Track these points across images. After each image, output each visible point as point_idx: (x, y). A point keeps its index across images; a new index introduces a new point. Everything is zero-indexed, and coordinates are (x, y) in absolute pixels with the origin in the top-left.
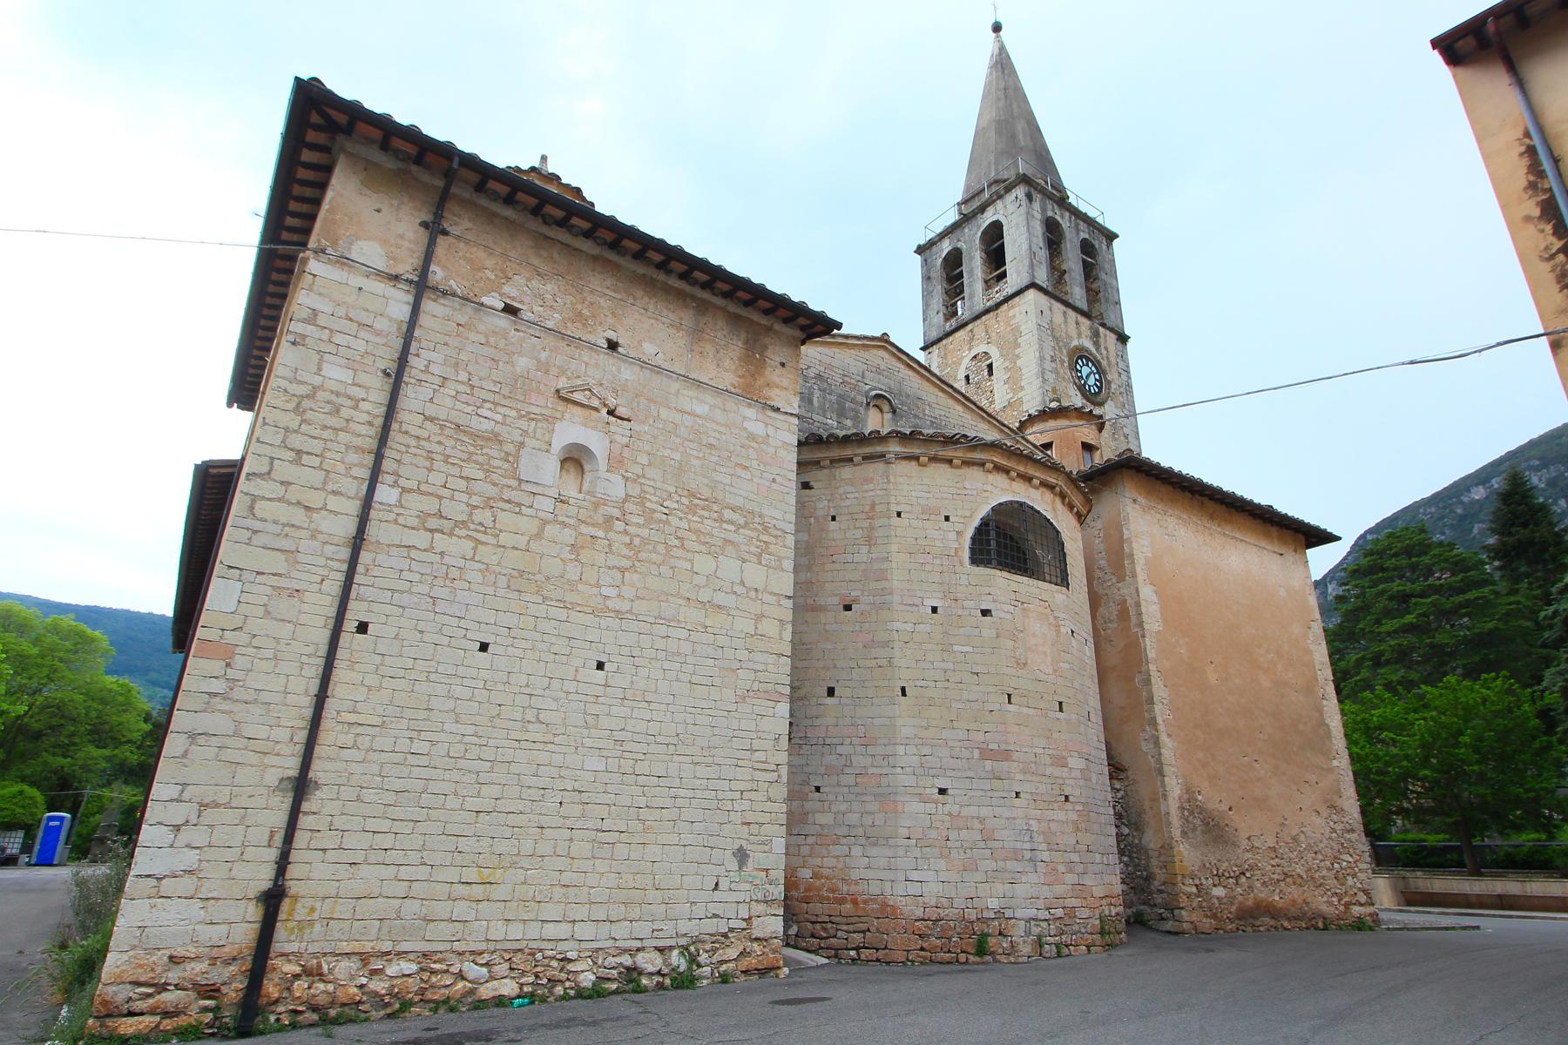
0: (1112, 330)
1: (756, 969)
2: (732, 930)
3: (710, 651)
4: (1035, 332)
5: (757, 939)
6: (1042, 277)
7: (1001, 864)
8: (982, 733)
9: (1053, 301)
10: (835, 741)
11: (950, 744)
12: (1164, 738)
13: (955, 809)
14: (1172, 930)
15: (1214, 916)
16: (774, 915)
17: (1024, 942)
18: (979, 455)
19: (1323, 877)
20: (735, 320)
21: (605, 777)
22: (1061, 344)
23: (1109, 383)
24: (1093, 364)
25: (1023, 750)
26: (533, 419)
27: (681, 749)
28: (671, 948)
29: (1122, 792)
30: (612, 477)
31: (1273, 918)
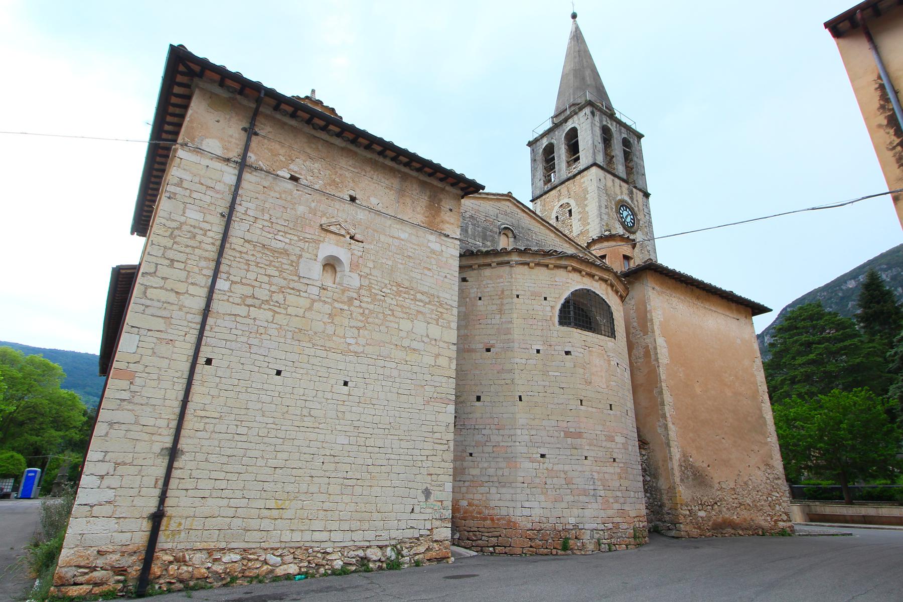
0: (640, 190)
1: (435, 558)
2: (421, 536)
3: (409, 375)
4: (596, 191)
5: (436, 541)
6: (600, 159)
7: (576, 498)
8: (565, 422)
9: (606, 174)
10: (481, 427)
11: (547, 428)
12: (670, 425)
13: (550, 466)
14: (675, 536)
15: (699, 528)
16: (446, 527)
17: (590, 543)
18: (564, 262)
19: (762, 505)
20: (423, 184)
21: (349, 448)
22: (611, 198)
23: (639, 220)
24: (630, 210)
25: (589, 432)
26: (307, 242)
27: (392, 432)
28: (386, 546)
29: (646, 457)
30: (352, 275)
31: (733, 529)
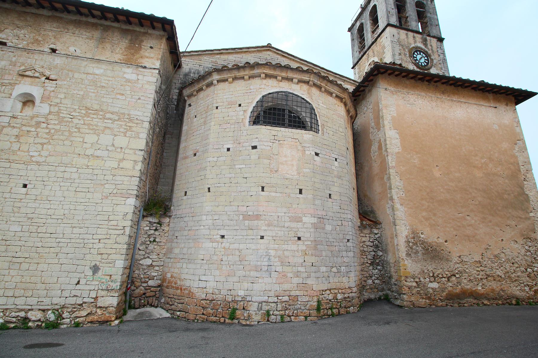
0: (434, 37)
1: (97, 321)
2: (85, 303)
3: (89, 177)
4: (390, 45)
6: (394, 20)
9: (400, 30)
12: (398, 206)
15: (429, 298)
16: (112, 296)
18: (256, 71)
19: (518, 276)
20: (125, 32)
21: (21, 234)
22: (404, 47)
23: (432, 60)
24: (423, 53)
26: (4, 85)
27: (65, 221)
28: (48, 310)
29: (379, 235)
30: (42, 105)
31: (475, 299)
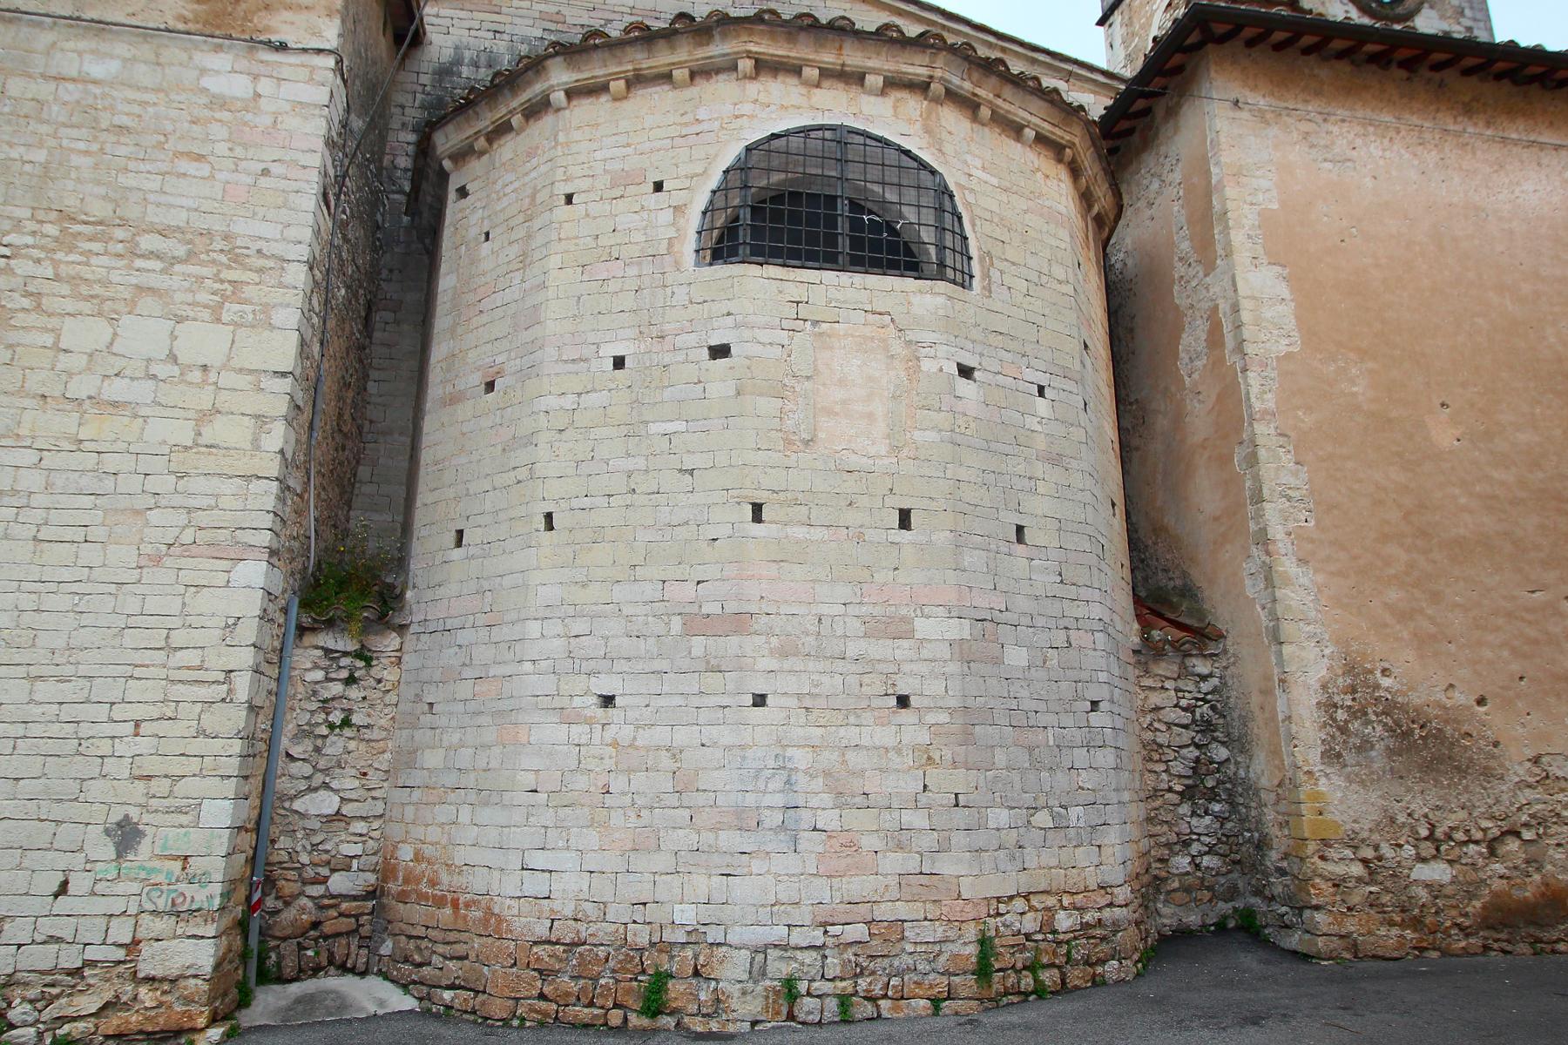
1: (141, 1032)
2: (92, 964)
5: (150, 979)
7: (708, 837)
8: (691, 586)
10: (456, 623)
11: (627, 610)
12: (1287, 565)
14: (1299, 949)
15: (1416, 923)
16: (194, 936)
18: (719, 49)
25: (784, 609)
29: (1215, 681)
